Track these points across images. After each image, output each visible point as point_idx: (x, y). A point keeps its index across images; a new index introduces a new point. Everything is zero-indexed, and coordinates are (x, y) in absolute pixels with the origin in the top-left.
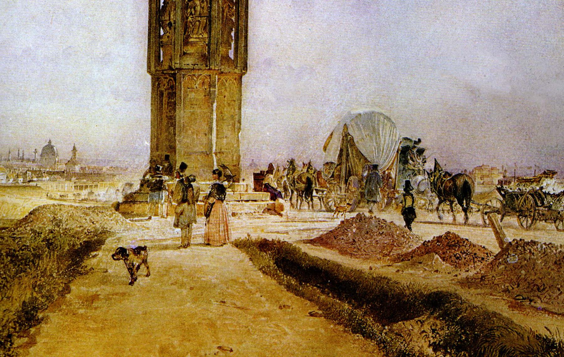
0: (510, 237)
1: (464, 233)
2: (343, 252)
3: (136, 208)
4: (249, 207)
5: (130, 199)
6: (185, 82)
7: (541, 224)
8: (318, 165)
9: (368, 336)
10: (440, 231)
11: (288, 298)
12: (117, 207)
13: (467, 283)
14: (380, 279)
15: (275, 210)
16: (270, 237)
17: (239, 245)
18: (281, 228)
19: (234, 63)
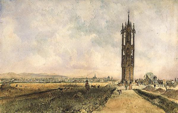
0: (168, 88)
1: (162, 88)
2: (146, 90)
3: (120, 85)
4: (134, 85)
5: (119, 84)
6: (126, 68)
7: (172, 87)
8: (143, 79)
9: (150, 101)
10: (159, 88)
11: (139, 96)
12: (117, 85)
13: (162, 94)
14: (151, 94)
15: (138, 85)
16: (137, 89)
17: (134, 90)
18: (138, 87)
19: (132, 66)
